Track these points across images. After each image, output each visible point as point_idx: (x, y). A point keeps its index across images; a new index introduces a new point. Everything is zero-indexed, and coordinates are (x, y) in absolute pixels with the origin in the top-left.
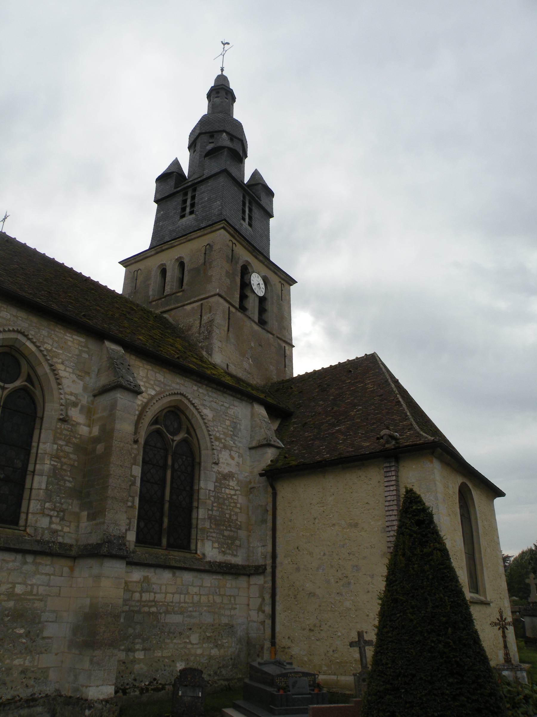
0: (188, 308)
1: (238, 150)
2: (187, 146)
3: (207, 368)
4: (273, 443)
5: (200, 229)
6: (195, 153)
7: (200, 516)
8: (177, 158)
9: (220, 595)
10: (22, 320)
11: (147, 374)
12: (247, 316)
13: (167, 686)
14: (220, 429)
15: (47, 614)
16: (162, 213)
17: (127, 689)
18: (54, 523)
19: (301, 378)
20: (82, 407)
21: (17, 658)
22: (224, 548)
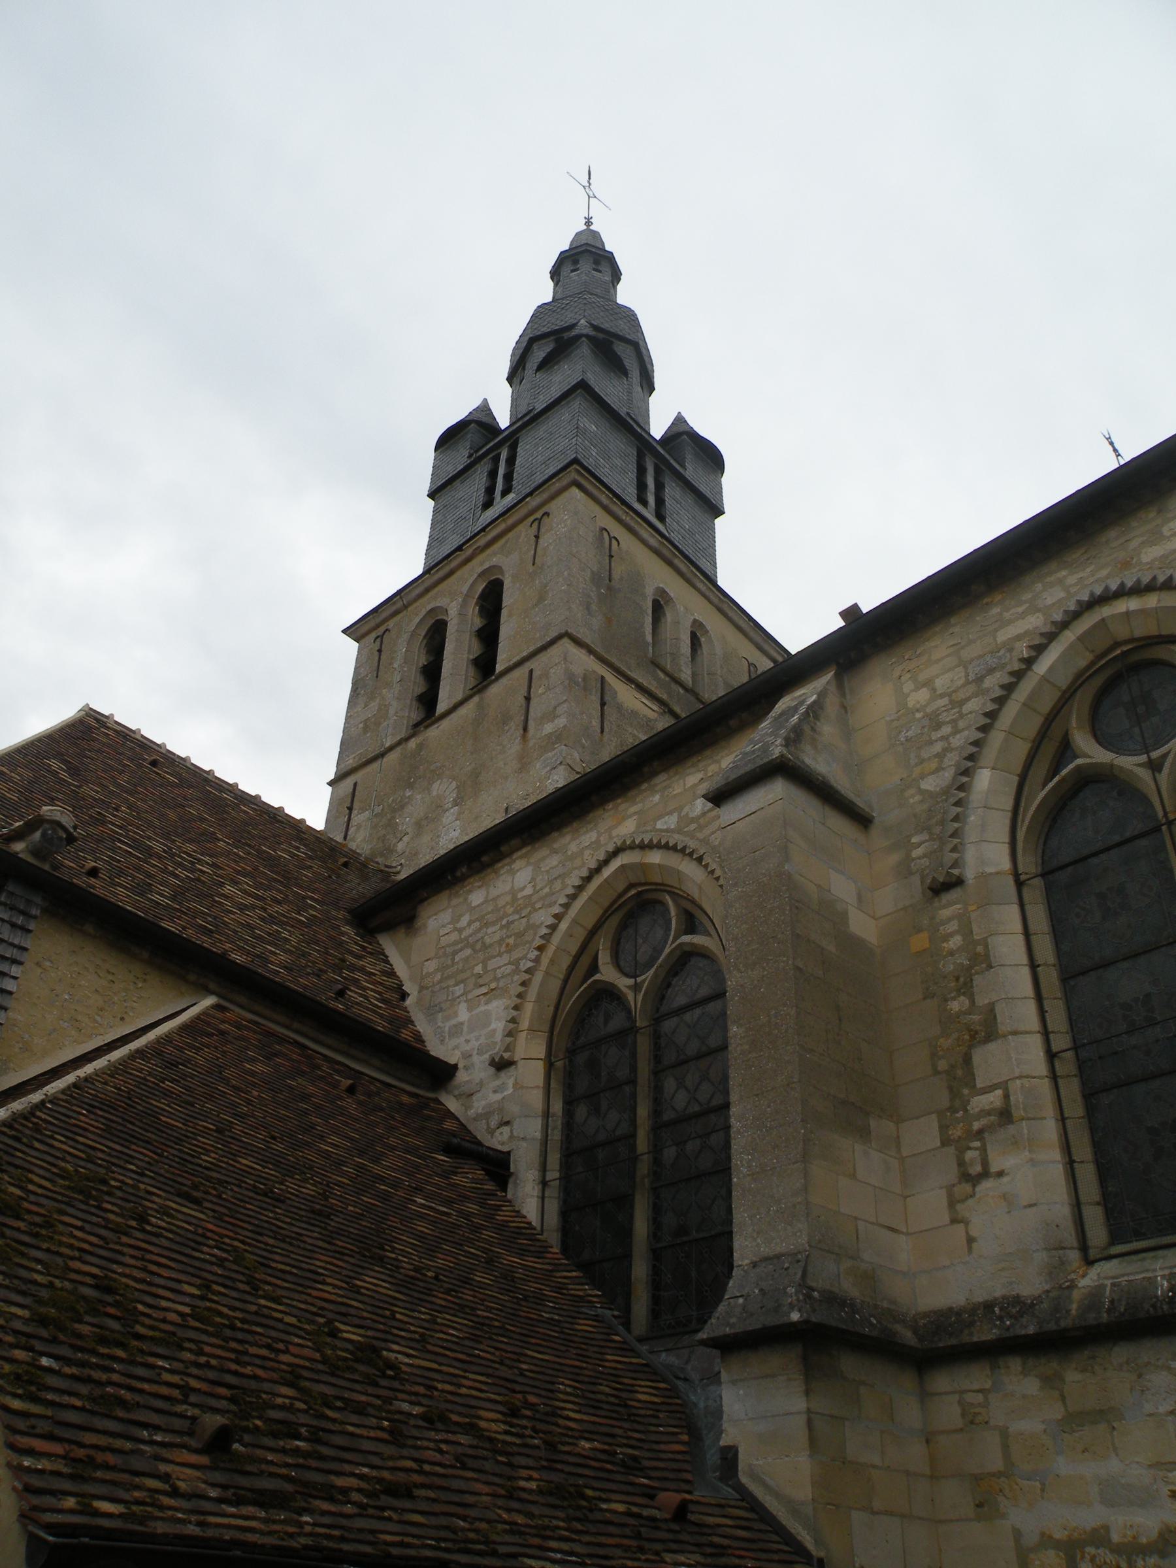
8: (485, 400)
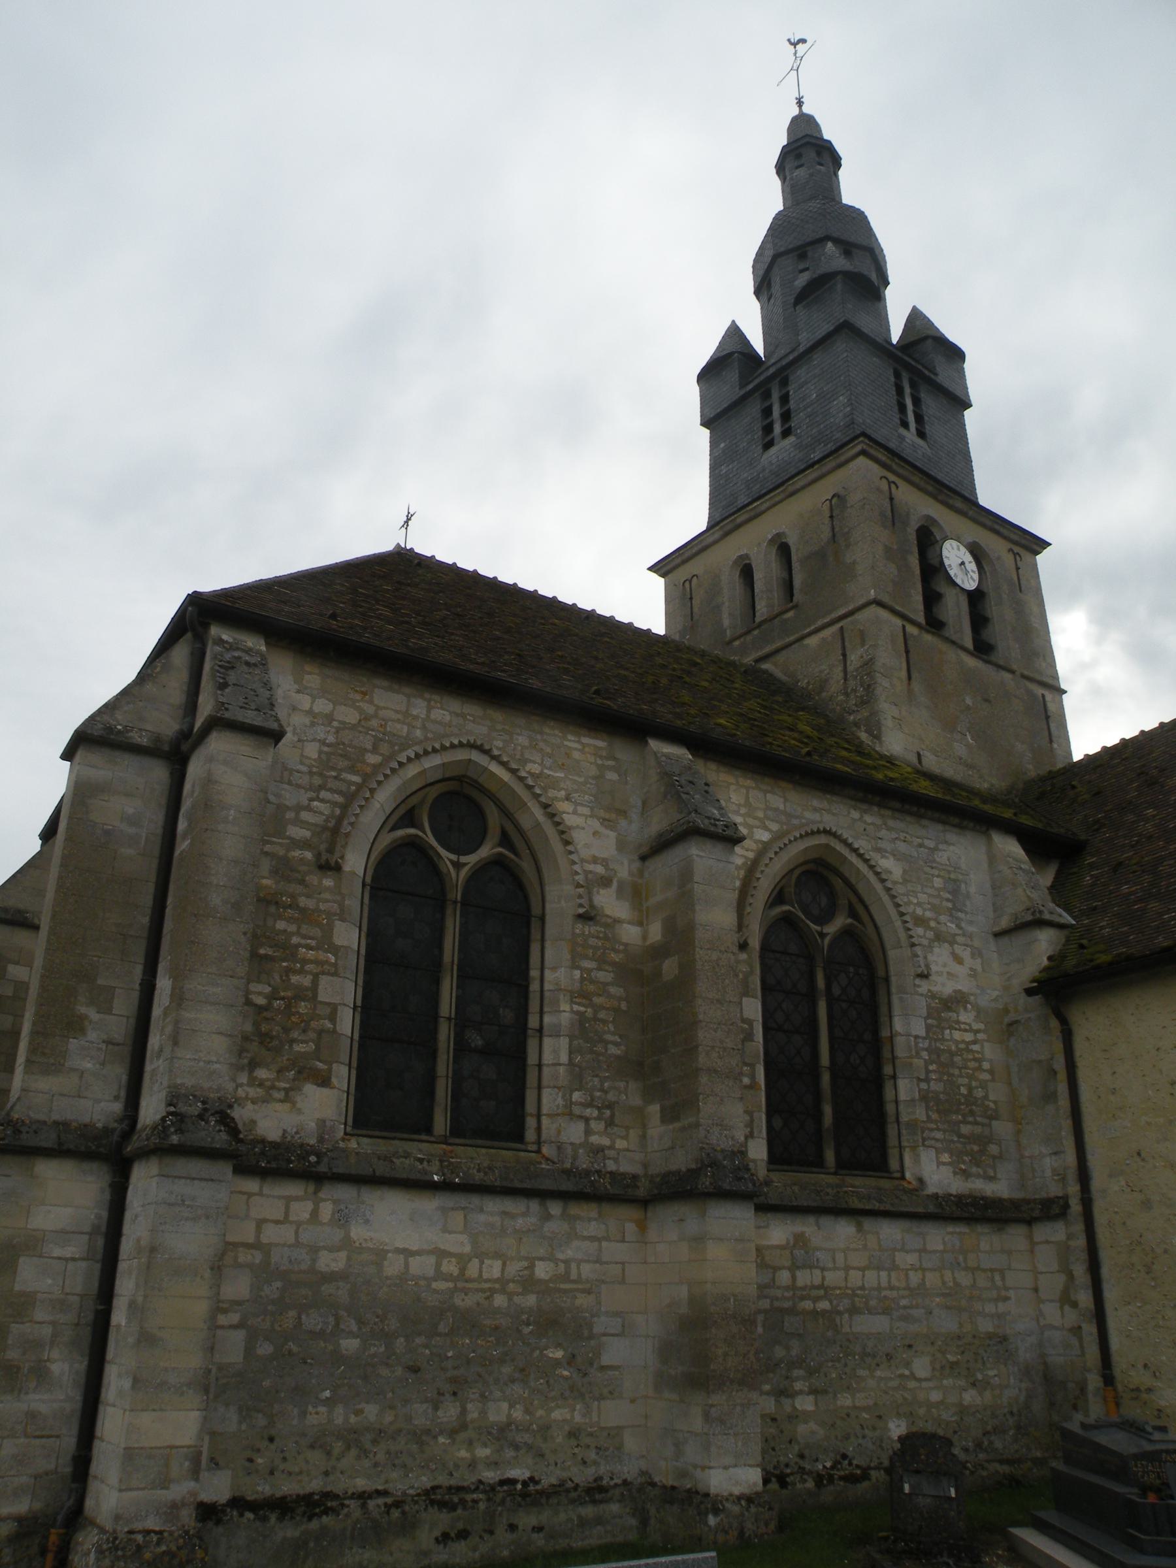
0: (813, 641)
1: (866, 273)
2: (752, 290)
3: (875, 768)
4: (1047, 916)
5: (812, 465)
6: (772, 301)
7: (902, 1096)
9: (966, 1268)
10: (473, 722)
11: (747, 798)
12: (947, 640)
13: (872, 1472)
14: (923, 898)
15: (603, 1318)
16: (722, 445)
17: (788, 1475)
18: (595, 1133)
19: (1091, 761)
20: (621, 884)
21: (558, 1407)
22: (964, 1162)
